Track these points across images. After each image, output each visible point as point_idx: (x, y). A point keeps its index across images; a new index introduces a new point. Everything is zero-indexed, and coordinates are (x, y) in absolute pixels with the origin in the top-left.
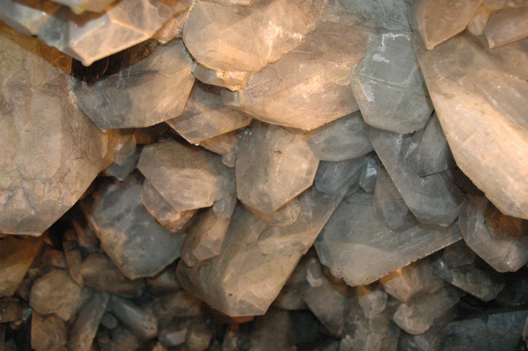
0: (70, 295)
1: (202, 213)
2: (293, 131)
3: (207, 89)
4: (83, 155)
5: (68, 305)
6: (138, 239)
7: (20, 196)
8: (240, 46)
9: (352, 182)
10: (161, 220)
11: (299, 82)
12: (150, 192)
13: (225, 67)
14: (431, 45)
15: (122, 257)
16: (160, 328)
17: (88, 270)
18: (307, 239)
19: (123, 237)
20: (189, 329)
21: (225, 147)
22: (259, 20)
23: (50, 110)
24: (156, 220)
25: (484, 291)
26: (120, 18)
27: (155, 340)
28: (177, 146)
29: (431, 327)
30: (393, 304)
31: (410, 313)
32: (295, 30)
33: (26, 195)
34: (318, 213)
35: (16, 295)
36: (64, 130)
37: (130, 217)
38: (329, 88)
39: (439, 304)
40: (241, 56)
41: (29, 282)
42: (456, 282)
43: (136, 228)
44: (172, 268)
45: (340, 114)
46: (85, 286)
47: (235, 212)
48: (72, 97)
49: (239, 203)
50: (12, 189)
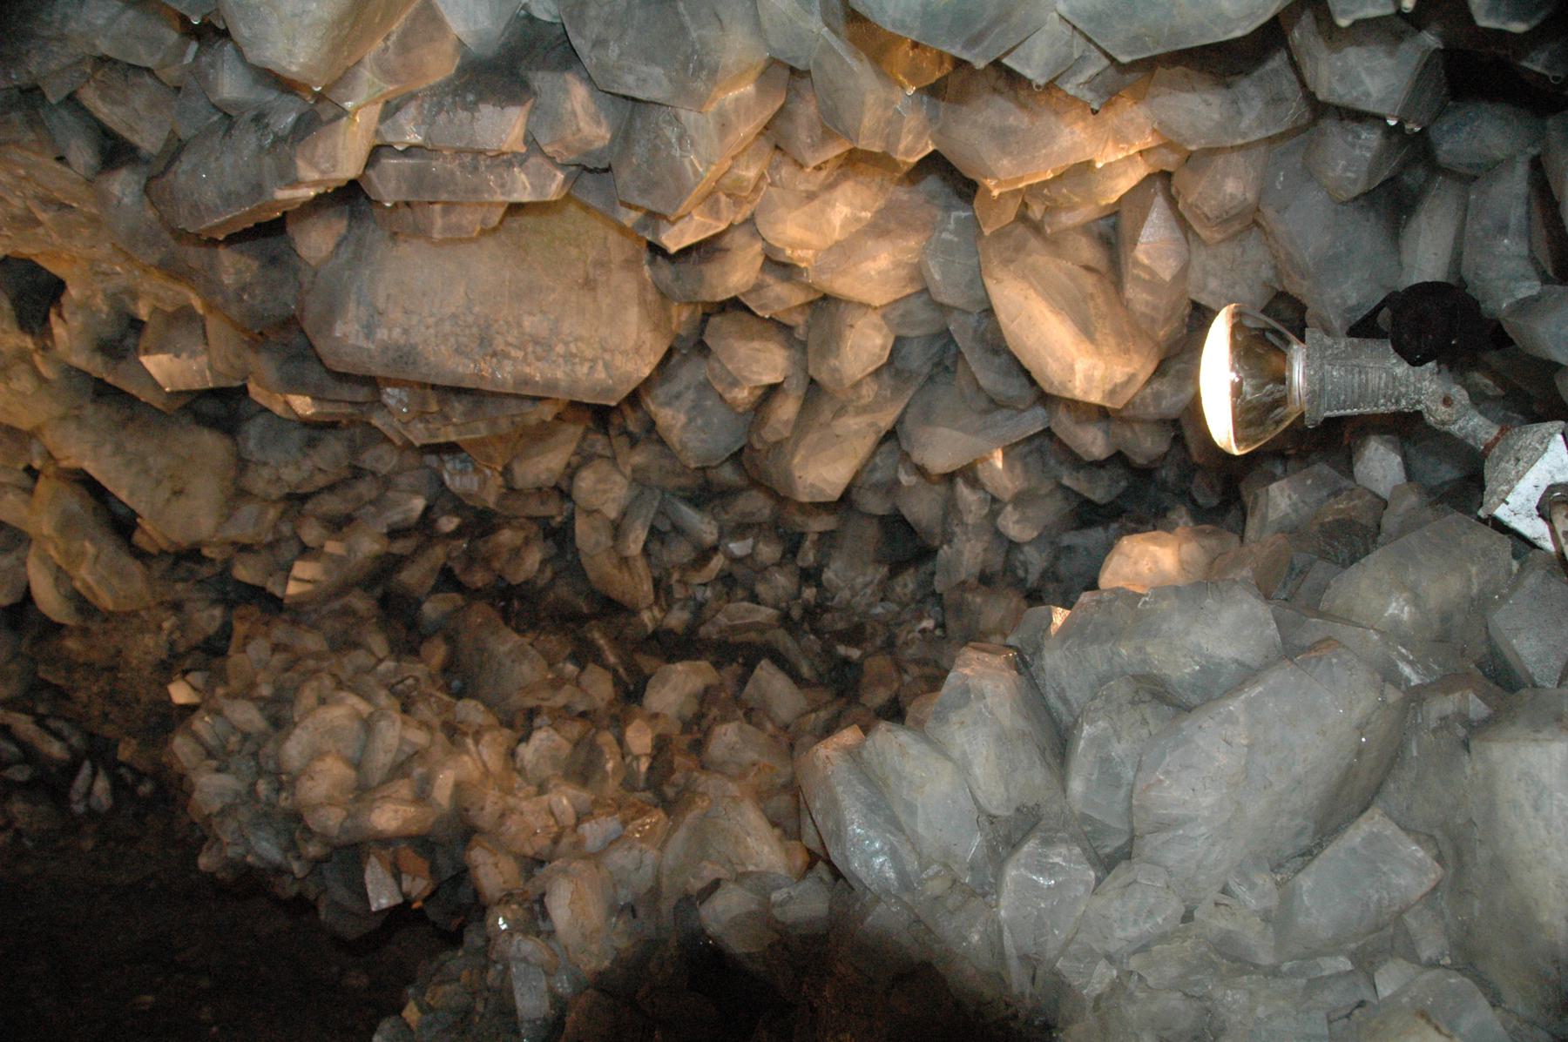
0: (616, 489)
1: (772, 390)
2: (864, 306)
3: (778, 265)
4: (656, 327)
5: (614, 500)
6: (699, 422)
7: (600, 366)
8: (807, 228)
9: (936, 360)
10: (727, 396)
11: (866, 259)
12: (717, 365)
13: (793, 247)
14: (987, 232)
15: (680, 441)
16: (721, 535)
17: (638, 458)
18: (886, 420)
19: (682, 418)
20: (756, 538)
21: (798, 320)
22: (827, 203)
23: (627, 285)
24: (721, 396)
25: (1099, 491)
26: (701, 215)
27: (715, 549)
28: (745, 316)
29: (1040, 536)
30: (996, 507)
31: (1016, 517)
32: (864, 208)
33: (607, 366)
34: (897, 391)
35: (556, 488)
36: (639, 304)
37: (691, 395)
38: (897, 265)
39: (1051, 508)
40: (813, 239)
41: (572, 472)
42: (1066, 481)
43: (697, 407)
44: (736, 458)
45: (909, 291)
46: (634, 480)
47: (808, 390)
48: (647, 271)
49: (812, 381)
50: (594, 361)
